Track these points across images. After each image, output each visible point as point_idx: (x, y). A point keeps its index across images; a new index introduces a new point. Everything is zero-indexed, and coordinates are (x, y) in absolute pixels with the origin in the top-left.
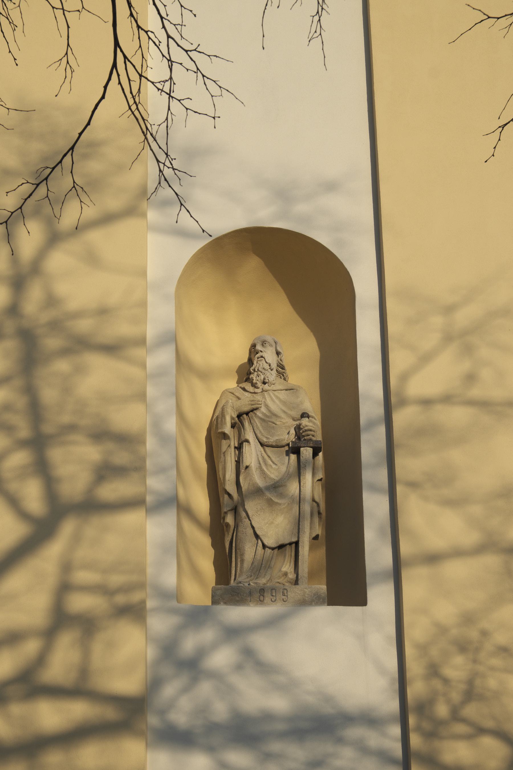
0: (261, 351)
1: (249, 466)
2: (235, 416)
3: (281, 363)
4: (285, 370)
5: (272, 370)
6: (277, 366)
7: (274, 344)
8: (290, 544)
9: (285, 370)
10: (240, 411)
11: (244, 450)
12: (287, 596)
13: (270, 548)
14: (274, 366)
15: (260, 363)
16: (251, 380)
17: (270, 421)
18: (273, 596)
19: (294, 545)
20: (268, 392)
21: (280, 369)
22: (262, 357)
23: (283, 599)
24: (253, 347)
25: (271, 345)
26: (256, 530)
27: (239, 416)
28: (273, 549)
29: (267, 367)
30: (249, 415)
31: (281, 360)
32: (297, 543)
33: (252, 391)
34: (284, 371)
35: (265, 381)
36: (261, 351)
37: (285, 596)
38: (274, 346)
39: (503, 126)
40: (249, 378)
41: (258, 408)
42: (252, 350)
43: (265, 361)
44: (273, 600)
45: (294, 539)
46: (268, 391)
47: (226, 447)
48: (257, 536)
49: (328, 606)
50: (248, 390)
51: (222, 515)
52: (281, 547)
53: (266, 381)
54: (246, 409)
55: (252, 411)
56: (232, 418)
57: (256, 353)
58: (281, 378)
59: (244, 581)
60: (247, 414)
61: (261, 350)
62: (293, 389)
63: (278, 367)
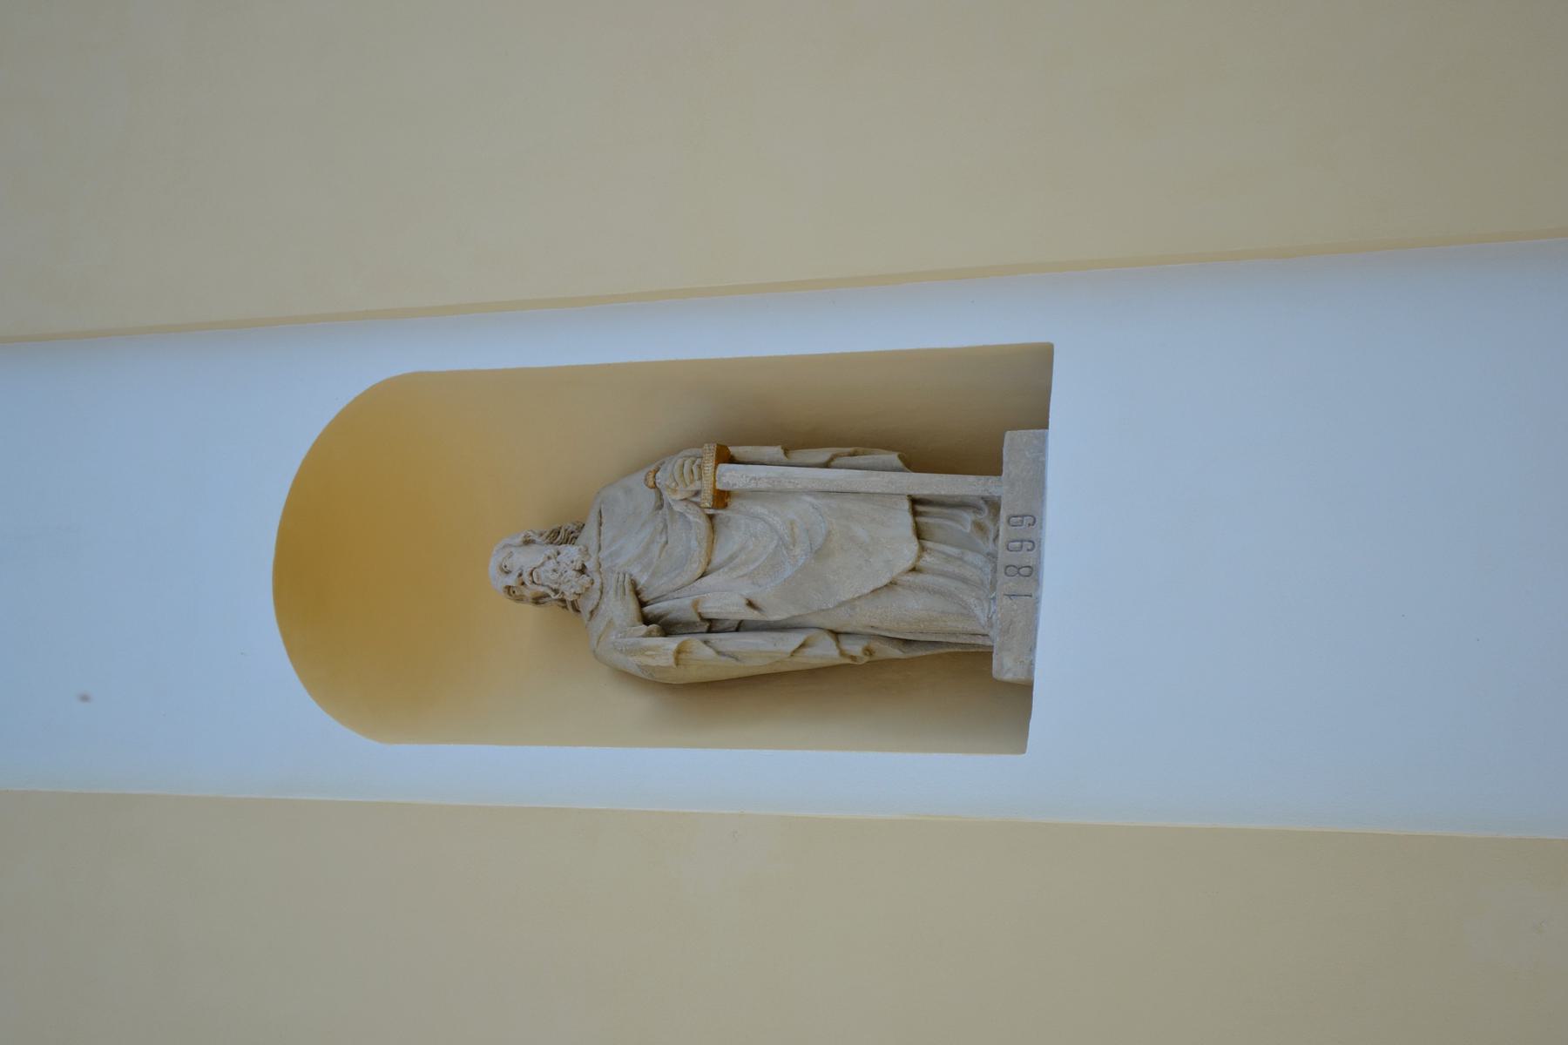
0: (520, 575)
1: (747, 599)
2: (644, 628)
3: (546, 535)
4: (560, 528)
5: (559, 554)
6: (552, 543)
7: (508, 550)
8: (915, 513)
9: (560, 528)
10: (636, 620)
11: (715, 610)
12: (1023, 516)
13: (919, 557)
14: (551, 550)
15: (543, 576)
16: (576, 597)
17: (660, 557)
18: (1022, 547)
19: (920, 508)
20: (603, 560)
21: (559, 538)
22: (531, 574)
23: (1029, 525)
24: (511, 592)
25: (511, 555)
26: (880, 584)
27: (646, 620)
28: (923, 549)
29: (551, 564)
30: (645, 599)
31: (541, 535)
32: (915, 501)
33: (596, 595)
34: (562, 531)
35: (648, 614)
36: (520, 575)
37: (1022, 521)
38: (513, 549)
39: (894, 652)
40: (573, 603)
41: (632, 580)
42: (516, 596)
43: (539, 567)
44: (1029, 547)
45: (906, 505)
46: (600, 560)
47: (707, 648)
48: (892, 584)
49: (1050, 427)
50: (595, 603)
51: (848, 661)
52: (919, 534)
53: (578, 566)
54: (633, 605)
55: (637, 593)
56: (649, 635)
57: (522, 587)
58: (576, 538)
59: (986, 611)
60: (642, 604)
61: (517, 574)
62: (600, 511)
63: (555, 542)
